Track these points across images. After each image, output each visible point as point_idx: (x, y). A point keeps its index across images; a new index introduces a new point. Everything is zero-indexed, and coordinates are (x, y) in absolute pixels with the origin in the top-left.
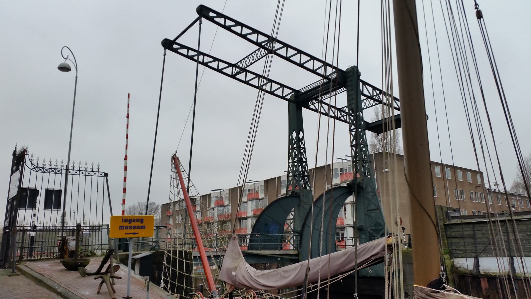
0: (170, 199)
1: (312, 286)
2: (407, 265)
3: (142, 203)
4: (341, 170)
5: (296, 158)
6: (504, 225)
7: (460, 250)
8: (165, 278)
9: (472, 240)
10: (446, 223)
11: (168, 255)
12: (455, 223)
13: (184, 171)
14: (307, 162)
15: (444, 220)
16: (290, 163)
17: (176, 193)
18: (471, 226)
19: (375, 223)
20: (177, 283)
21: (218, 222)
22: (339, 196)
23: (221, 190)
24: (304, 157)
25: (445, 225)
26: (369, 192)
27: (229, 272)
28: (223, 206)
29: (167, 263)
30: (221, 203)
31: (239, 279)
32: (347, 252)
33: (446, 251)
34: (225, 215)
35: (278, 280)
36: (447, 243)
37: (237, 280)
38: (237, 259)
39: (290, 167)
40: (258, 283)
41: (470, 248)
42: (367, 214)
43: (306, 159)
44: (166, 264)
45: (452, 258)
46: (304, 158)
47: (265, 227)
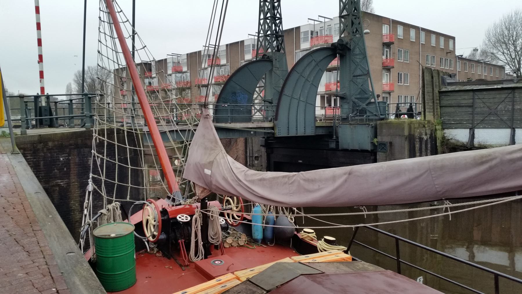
0: (99, 52)
1: (367, 213)
2: (397, 137)
3: (92, 67)
4: (312, 33)
5: (269, 13)
6: (510, 93)
7: (454, 120)
8: (96, 176)
9: (470, 110)
10: (442, 90)
11: (99, 139)
12: (453, 90)
13: (121, 11)
14: (282, 18)
15: (439, 87)
16: (262, 19)
17: (109, 44)
18: (471, 94)
19: (359, 90)
20: (116, 182)
21: (177, 89)
22: (322, 59)
23: (178, 55)
24: (278, 12)
25: (440, 93)
26: (357, 55)
27: (199, 169)
28: (181, 72)
29: (98, 152)
30: (179, 69)
31: (217, 181)
32: (490, 158)
33: (438, 122)
34: (184, 82)
35: (291, 193)
36: (440, 112)
37: (214, 183)
38: (212, 149)
39: (262, 24)
40: (251, 191)
41: (466, 118)
42: (352, 81)
43: (280, 15)
44: (96, 154)
45: (443, 129)
46: (278, 14)
47: (232, 96)
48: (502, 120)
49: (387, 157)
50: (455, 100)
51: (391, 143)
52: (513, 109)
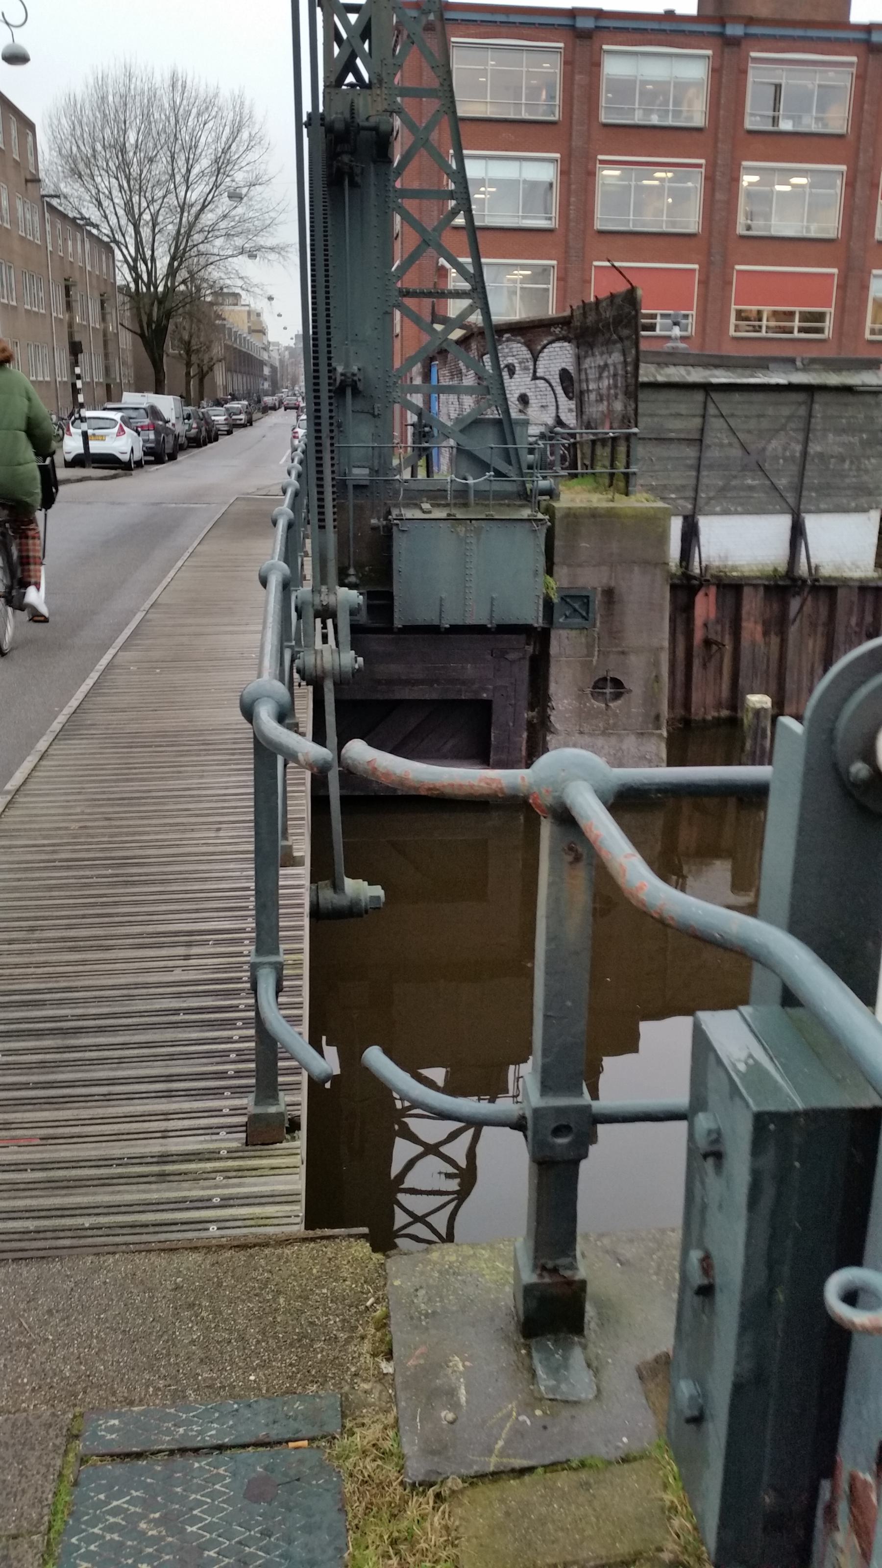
18: (699, 396)
41: (678, 482)
48: (774, 487)
49: (593, 646)
50: (651, 415)
51: (609, 594)
52: (805, 453)
